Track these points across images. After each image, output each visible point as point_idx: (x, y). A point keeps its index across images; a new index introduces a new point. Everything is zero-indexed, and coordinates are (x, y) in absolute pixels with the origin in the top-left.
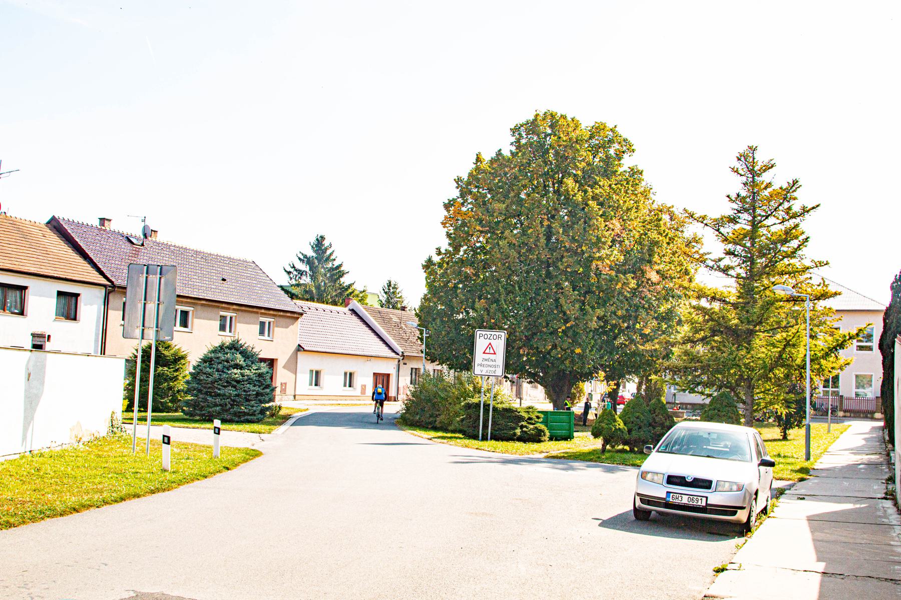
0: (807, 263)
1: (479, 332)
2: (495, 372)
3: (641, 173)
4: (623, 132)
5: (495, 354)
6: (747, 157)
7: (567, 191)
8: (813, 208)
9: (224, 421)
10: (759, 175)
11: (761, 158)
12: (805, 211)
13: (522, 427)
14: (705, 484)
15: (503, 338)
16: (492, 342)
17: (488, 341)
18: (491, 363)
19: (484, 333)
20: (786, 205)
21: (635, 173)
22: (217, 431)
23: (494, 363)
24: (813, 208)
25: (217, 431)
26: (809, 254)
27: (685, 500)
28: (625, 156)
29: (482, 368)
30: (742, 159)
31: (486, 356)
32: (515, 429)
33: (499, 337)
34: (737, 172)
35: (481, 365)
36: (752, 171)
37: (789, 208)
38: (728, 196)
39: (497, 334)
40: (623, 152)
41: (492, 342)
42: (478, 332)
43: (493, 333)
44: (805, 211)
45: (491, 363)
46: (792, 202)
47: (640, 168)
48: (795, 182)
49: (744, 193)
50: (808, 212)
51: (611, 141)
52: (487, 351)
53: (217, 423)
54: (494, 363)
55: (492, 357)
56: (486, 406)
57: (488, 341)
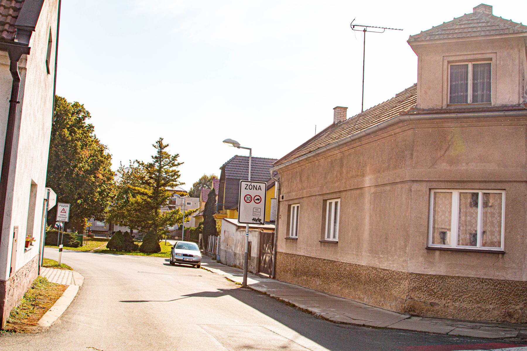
0: (178, 183)
1: (59, 204)
2: (65, 220)
3: (93, 128)
4: (87, 108)
5: (65, 213)
6: (160, 143)
7: (65, 134)
8: (182, 163)
9: (65, 245)
10: (163, 149)
11: (164, 143)
12: (179, 164)
13: (72, 241)
14: (191, 256)
15: (69, 207)
16: (65, 208)
17: (63, 208)
18: (64, 216)
19: (61, 204)
20: (173, 162)
21: (91, 127)
22: (61, 250)
23: (65, 216)
24: (182, 163)
25: (61, 250)
26: (180, 180)
27: (188, 260)
28: (86, 119)
29: (60, 218)
30: (158, 143)
31: (62, 213)
32: (70, 242)
33: (67, 206)
34: (155, 146)
35: (60, 217)
36: (160, 146)
37: (174, 163)
38: (152, 156)
39: (67, 205)
40: (86, 117)
41: (65, 208)
42: (69, 205)
43: (65, 205)
44: (179, 164)
45: (64, 216)
46: (175, 161)
47: (93, 125)
48: (178, 155)
49: (158, 156)
50: (180, 165)
51: (80, 111)
52: (62, 212)
53: (61, 246)
54: (65, 216)
55: (64, 214)
56: (61, 234)
57: (63, 208)
